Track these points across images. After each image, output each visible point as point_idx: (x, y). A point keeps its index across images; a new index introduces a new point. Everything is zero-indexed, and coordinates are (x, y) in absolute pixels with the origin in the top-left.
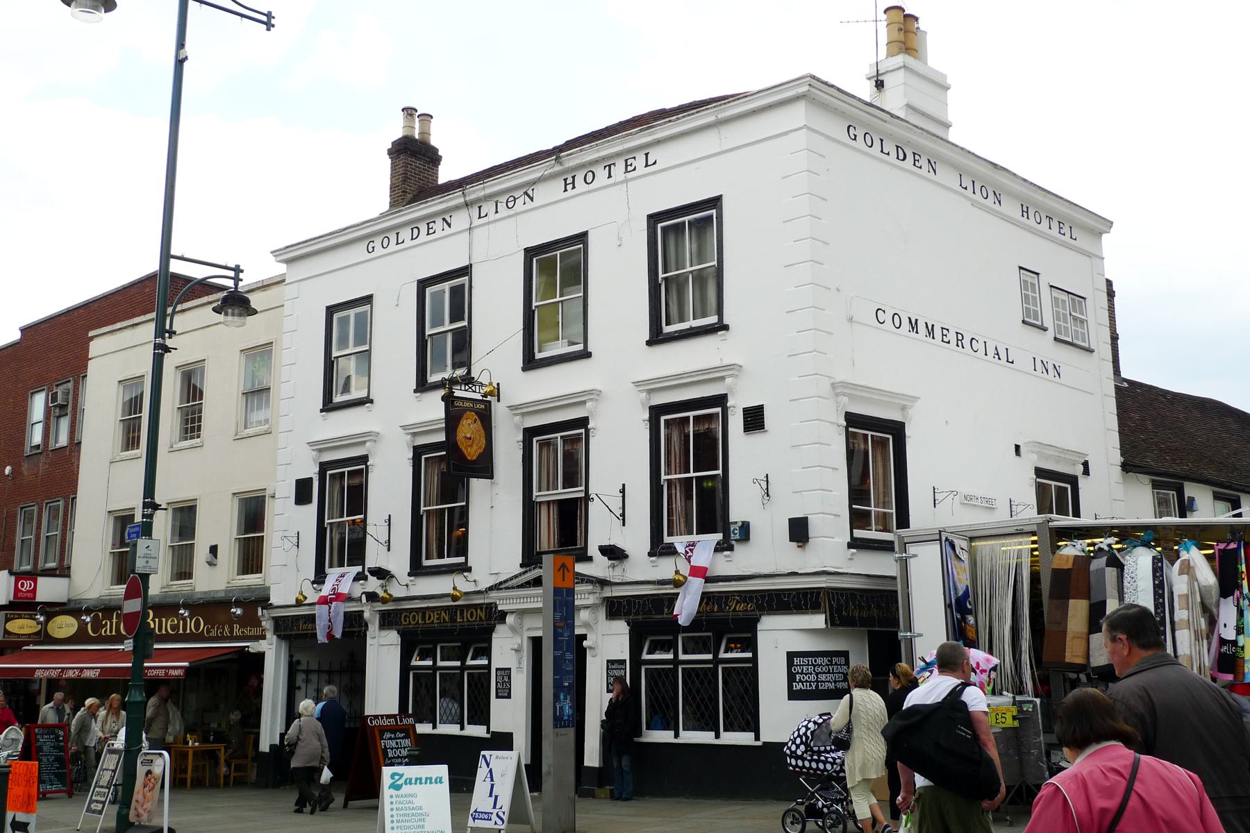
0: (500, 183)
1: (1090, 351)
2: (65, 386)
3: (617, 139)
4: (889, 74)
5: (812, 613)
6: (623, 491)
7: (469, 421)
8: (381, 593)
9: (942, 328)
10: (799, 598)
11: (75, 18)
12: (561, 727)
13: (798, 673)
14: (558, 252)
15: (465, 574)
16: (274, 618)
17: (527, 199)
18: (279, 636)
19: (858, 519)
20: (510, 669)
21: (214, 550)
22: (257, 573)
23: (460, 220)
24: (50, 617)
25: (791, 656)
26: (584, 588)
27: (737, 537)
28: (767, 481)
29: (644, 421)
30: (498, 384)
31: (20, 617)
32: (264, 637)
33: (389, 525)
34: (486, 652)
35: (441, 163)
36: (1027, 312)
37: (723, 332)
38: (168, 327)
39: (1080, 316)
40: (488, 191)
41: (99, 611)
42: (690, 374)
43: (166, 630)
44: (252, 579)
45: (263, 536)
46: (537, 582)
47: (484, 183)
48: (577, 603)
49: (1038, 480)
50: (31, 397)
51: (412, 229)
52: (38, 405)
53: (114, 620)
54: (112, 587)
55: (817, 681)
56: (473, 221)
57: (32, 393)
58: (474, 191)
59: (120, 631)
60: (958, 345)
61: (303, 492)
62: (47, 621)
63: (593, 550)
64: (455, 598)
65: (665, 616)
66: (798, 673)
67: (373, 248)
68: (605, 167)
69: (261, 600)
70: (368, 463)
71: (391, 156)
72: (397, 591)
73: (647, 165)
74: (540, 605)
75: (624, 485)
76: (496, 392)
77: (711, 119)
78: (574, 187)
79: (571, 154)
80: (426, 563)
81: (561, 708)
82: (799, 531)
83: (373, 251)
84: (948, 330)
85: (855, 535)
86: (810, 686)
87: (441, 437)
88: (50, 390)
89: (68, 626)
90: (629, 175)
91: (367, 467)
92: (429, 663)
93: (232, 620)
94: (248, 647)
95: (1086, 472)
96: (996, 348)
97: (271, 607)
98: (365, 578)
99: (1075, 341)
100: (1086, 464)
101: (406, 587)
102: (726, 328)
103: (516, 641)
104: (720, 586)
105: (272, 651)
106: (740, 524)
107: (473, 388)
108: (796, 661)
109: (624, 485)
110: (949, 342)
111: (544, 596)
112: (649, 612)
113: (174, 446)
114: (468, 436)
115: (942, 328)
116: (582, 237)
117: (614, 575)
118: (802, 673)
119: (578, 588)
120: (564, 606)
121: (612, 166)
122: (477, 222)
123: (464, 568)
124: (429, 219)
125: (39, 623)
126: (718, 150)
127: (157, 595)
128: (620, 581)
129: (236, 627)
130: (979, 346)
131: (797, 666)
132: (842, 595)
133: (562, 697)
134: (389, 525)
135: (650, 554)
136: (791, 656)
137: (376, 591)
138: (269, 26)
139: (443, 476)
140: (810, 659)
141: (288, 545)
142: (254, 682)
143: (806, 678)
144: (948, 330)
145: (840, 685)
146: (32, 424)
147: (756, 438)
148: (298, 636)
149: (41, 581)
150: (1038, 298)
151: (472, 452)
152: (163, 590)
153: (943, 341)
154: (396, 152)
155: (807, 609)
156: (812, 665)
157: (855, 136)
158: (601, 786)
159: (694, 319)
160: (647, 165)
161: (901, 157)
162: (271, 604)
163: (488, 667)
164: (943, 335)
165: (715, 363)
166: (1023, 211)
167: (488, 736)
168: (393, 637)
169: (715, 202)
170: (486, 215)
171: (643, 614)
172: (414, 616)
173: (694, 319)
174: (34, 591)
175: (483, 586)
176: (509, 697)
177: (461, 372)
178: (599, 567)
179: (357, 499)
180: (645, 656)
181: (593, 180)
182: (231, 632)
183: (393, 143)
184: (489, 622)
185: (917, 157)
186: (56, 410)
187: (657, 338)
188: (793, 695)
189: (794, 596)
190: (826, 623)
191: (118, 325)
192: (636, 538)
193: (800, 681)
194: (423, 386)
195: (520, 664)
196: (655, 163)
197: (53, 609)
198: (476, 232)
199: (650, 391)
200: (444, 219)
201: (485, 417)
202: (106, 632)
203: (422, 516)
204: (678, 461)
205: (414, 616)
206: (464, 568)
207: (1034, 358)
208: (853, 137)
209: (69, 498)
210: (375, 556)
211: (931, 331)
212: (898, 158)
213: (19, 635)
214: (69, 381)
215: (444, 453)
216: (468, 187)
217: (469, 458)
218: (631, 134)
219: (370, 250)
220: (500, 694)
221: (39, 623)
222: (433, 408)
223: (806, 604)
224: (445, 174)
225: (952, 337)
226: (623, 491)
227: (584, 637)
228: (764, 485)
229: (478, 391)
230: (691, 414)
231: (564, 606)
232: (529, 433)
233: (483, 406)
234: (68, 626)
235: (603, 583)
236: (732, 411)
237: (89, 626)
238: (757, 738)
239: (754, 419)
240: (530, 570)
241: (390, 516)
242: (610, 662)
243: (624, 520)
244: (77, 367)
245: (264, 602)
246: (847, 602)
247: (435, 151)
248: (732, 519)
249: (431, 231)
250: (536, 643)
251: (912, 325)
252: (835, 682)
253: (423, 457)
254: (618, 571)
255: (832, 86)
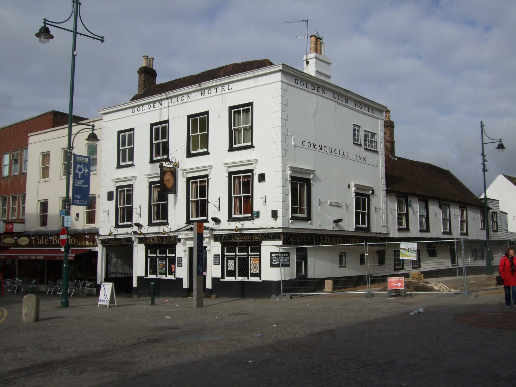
0: (179, 92)
1: (377, 152)
2: (17, 152)
3: (219, 79)
4: (310, 59)
5: (278, 240)
6: (219, 200)
7: (168, 175)
8: (138, 231)
9: (325, 147)
10: (274, 236)
11: (42, 43)
12: (199, 275)
13: (273, 259)
14: (199, 117)
15: (167, 226)
16: (101, 239)
17: (188, 97)
18: (103, 246)
19: (294, 210)
20: (182, 257)
21: (77, 215)
22: (93, 223)
23: (165, 103)
24: (19, 237)
25: (271, 254)
26: (206, 231)
27: (256, 216)
28: (265, 198)
29: (227, 177)
30: (178, 162)
31: (8, 237)
32: (97, 246)
33: (141, 209)
34: (174, 252)
35: (157, 76)
36: (355, 140)
37: (253, 148)
38: (72, 146)
39: (374, 140)
40: (175, 94)
41: (37, 236)
42: (242, 162)
43: (71, 243)
44: (91, 226)
45: (95, 211)
46: (191, 229)
47: (173, 91)
48: (204, 236)
49: (356, 196)
50: (4, 155)
51: (148, 105)
52: (6, 159)
53: (43, 239)
54: (41, 227)
55: (279, 261)
56: (170, 104)
57: (4, 154)
58: (170, 94)
59: (45, 242)
60: (330, 152)
61: (110, 196)
62: (18, 239)
63: (210, 219)
64: (164, 234)
65: (232, 241)
66: (273, 259)
67: (134, 111)
68: (215, 89)
69: (95, 233)
70: (133, 187)
71: (139, 74)
72: (144, 231)
73: (229, 89)
74: (193, 237)
75: (220, 198)
76: (177, 165)
77: (251, 75)
78: (204, 95)
79: (203, 84)
80: (153, 222)
81: (199, 270)
82: (274, 214)
83: (134, 112)
84: (327, 147)
85: (293, 215)
86: (277, 263)
87: (158, 179)
88: (11, 153)
89: (25, 241)
90: (223, 92)
91: (133, 188)
92: (155, 255)
93: (87, 239)
94: (92, 249)
95: (373, 193)
96: (343, 152)
97: (100, 235)
98: (133, 226)
99: (372, 149)
100: (373, 191)
101: (146, 229)
102: (253, 147)
103: (184, 248)
104: (250, 231)
105: (100, 250)
106: (256, 212)
107: (170, 163)
108: (273, 255)
109: (220, 198)
110: (327, 151)
111: (194, 233)
112: (227, 239)
113: (62, 177)
114: (168, 180)
115: (325, 147)
116: (207, 113)
117: (216, 227)
118: (274, 259)
119: (204, 231)
120: (200, 238)
121: (217, 89)
122: (171, 104)
123: (166, 224)
124: (154, 102)
125: (15, 239)
126: (254, 86)
127: (57, 230)
128: (218, 229)
129: (87, 242)
130: (337, 152)
131: (273, 257)
132: (288, 235)
133: (199, 266)
134: (141, 209)
135: (228, 221)
136: (271, 254)
137: (136, 231)
138: (103, 41)
139: (159, 193)
140: (277, 255)
141: (105, 214)
142: (94, 261)
143: (276, 260)
144: (327, 147)
145: (286, 263)
146: (5, 166)
147: (262, 184)
148: (109, 246)
149: (15, 225)
150: (359, 135)
151: (169, 185)
152: (60, 229)
153: (325, 151)
154: (141, 72)
155: (277, 239)
156: (278, 256)
157: (298, 83)
158: (211, 294)
159: (243, 143)
160: (229, 89)
161: (313, 89)
162: (100, 235)
163: (175, 257)
164: (325, 149)
165: (250, 158)
166: (355, 105)
167: (175, 279)
168: (142, 246)
169: (251, 104)
170: (174, 102)
171: (226, 240)
172: (150, 240)
173: (243, 143)
174: (12, 228)
175: (173, 230)
176: (182, 266)
177: (166, 157)
178: (211, 224)
179: (129, 199)
180: (226, 254)
181: (211, 92)
182: (85, 243)
183: (139, 69)
184: (175, 242)
185: (319, 88)
186: (15, 161)
187: (231, 149)
188: (272, 266)
189: (272, 235)
190: (282, 243)
191: (39, 132)
192: (223, 215)
193: (274, 261)
194: (152, 161)
195: (185, 256)
196: (231, 89)
197: (20, 235)
198: (170, 108)
199: (229, 167)
200: (159, 103)
201: (174, 173)
202: (39, 243)
203: (152, 206)
204: (237, 190)
205: (150, 240)
206: (166, 224)
207: (357, 155)
208: (297, 83)
209: (20, 194)
210: (135, 219)
211: (321, 148)
212: (312, 89)
213: (8, 244)
214: (19, 150)
215: (160, 184)
216: (168, 92)
217: (168, 187)
218: (224, 78)
219: (133, 112)
220: (179, 265)
221: (15, 239)
222: (156, 169)
223: (276, 238)
224: (160, 80)
225: (328, 149)
226: (219, 200)
227: (206, 247)
228: (264, 199)
229: (171, 164)
230: (242, 175)
231: (200, 238)
232: (189, 179)
233: (173, 170)
234: (25, 241)
235: (213, 230)
236: (255, 175)
237: (33, 241)
238: (260, 279)
239: (262, 178)
240: (189, 225)
241: (141, 205)
242: (215, 255)
243: (220, 209)
244: (24, 145)
245: (97, 233)
246: (289, 237)
247: (155, 71)
248: (254, 210)
249: (155, 106)
250: (191, 249)
251: (314, 146)
252: (285, 262)
253: (152, 186)
254: (218, 226)
255: (290, 67)
